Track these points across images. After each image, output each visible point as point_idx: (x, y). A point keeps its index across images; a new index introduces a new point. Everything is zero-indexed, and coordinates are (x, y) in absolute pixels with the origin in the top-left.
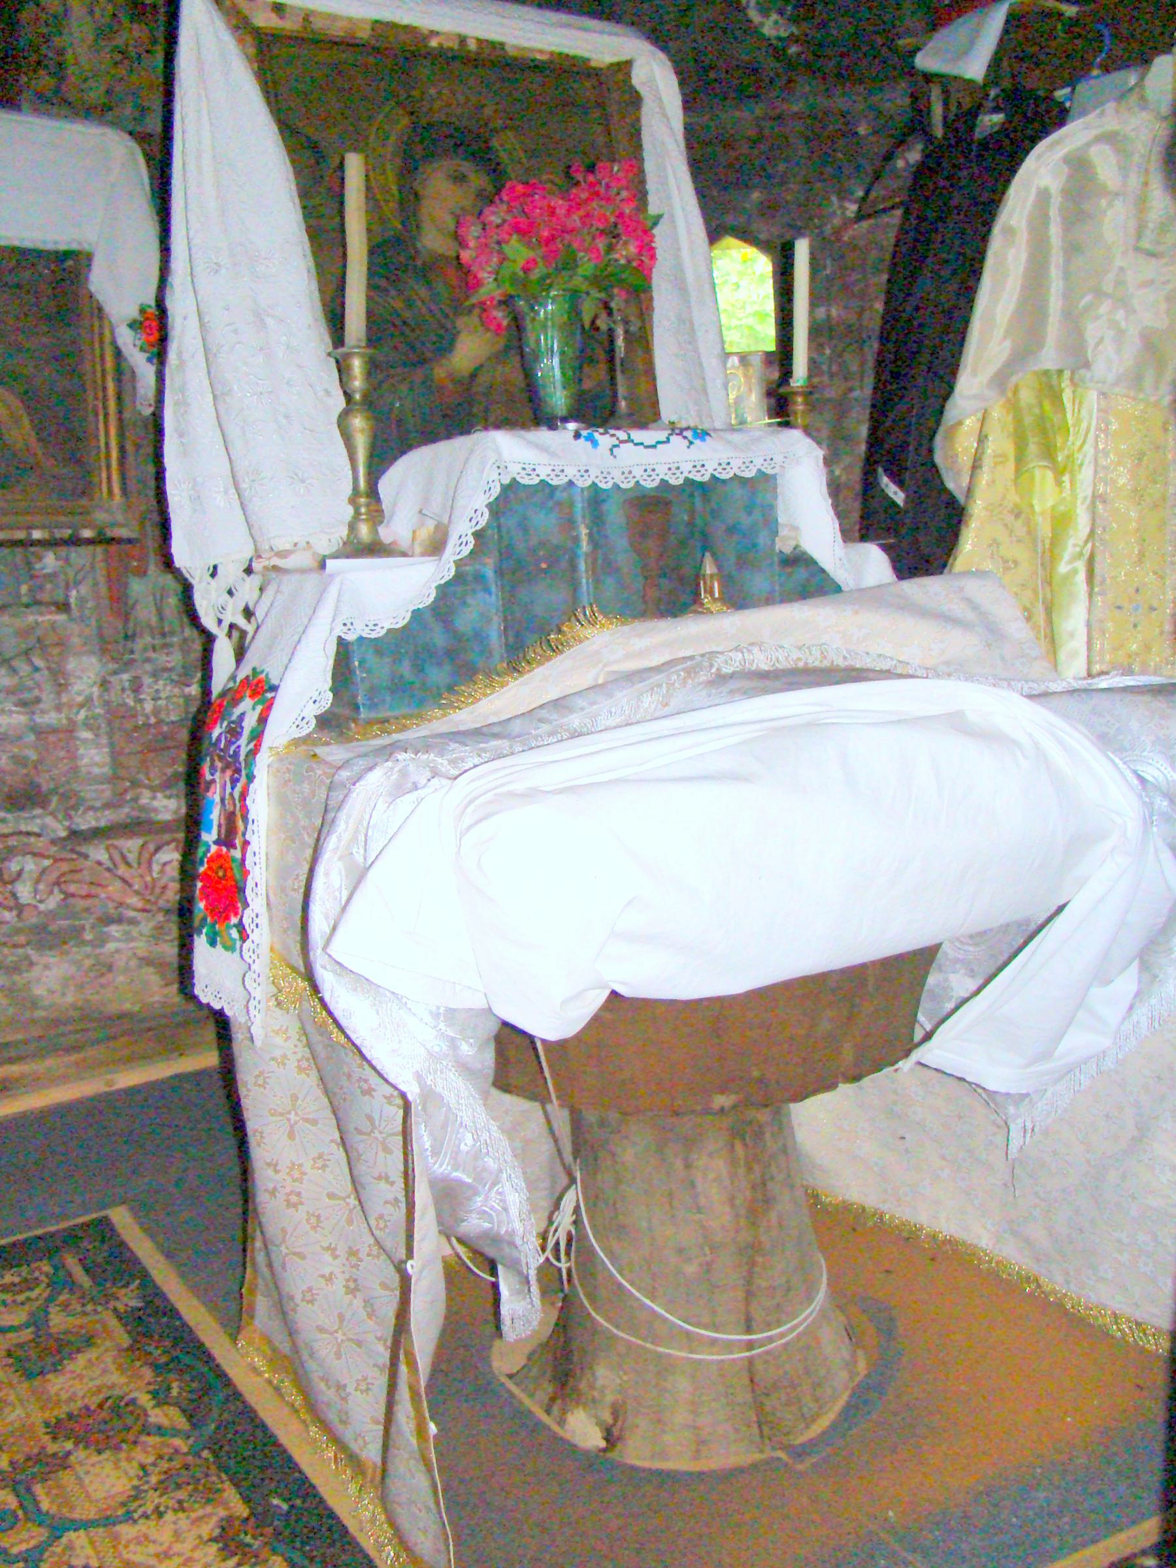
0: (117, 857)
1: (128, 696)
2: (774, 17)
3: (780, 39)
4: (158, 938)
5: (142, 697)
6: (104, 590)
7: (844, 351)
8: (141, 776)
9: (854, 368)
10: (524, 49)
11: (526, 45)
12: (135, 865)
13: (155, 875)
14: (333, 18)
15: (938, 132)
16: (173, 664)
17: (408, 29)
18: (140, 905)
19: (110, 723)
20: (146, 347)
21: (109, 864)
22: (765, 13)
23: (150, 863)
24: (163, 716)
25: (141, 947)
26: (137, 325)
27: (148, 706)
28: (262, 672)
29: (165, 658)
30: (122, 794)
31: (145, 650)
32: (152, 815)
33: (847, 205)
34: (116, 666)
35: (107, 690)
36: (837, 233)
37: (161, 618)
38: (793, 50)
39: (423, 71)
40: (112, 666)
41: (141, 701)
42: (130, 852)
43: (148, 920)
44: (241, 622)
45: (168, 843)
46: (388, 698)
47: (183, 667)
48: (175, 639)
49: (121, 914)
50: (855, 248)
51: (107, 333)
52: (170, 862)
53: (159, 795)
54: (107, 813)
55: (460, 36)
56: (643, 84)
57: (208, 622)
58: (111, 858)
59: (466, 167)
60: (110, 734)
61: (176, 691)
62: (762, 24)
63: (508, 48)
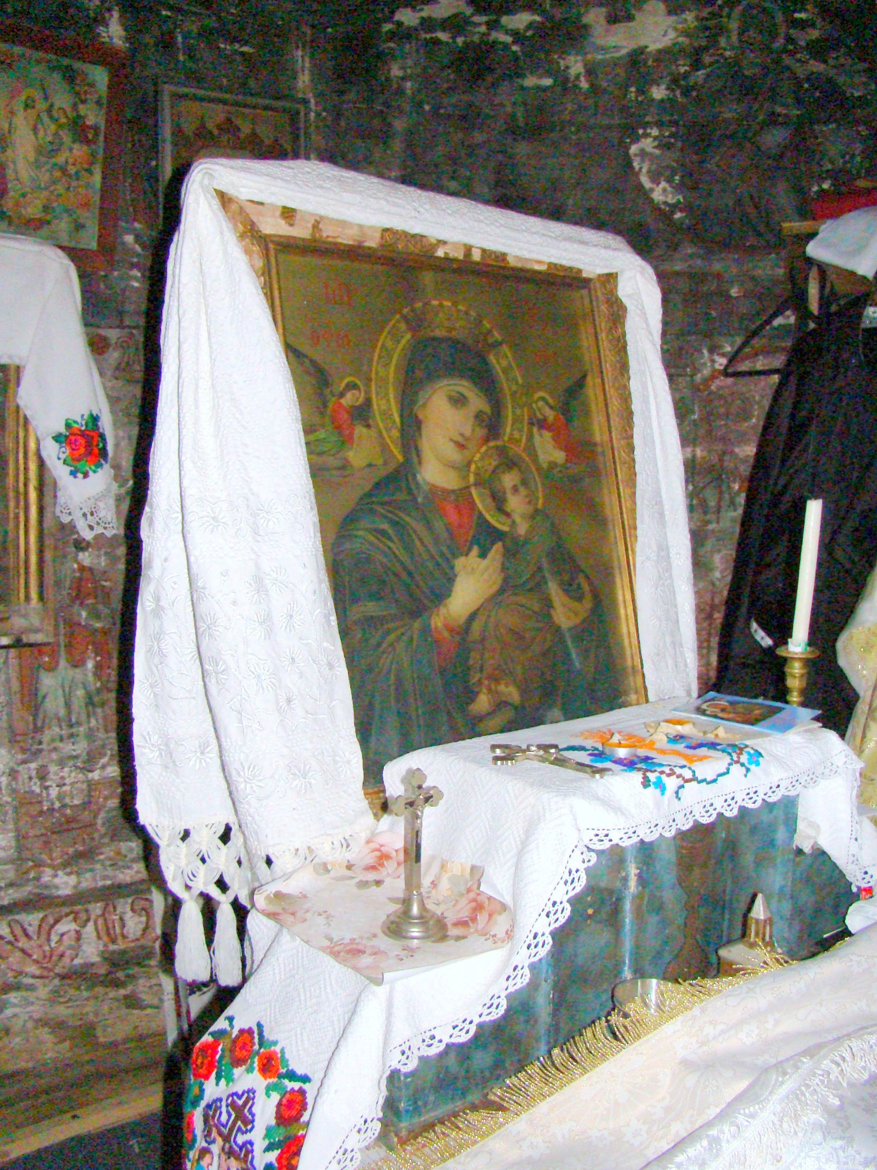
0: (18, 931)
1: (35, 784)
2: (663, 184)
3: (665, 203)
4: (54, 1001)
5: (48, 784)
6: (15, 686)
7: (704, 487)
8: (44, 857)
9: (712, 503)
10: (527, 260)
11: (527, 256)
12: (35, 938)
13: (53, 944)
14: (343, 224)
15: (814, 306)
16: (79, 752)
17: (419, 238)
18: (38, 972)
19: (16, 810)
20: (69, 461)
21: (10, 937)
22: (656, 180)
23: (49, 934)
24: (67, 800)
25: (37, 1010)
26: (63, 439)
27: (54, 792)
28: (275, 1043)
29: (71, 747)
30: (25, 873)
31: (53, 740)
32: (54, 891)
33: (716, 358)
34: (24, 756)
35: (15, 779)
36: (707, 382)
37: (68, 705)
38: (678, 215)
39: (428, 278)
40: (20, 757)
41: (47, 788)
42: (30, 925)
43: (45, 986)
44: (214, 892)
45: (67, 915)
46: (432, 1098)
47: (88, 754)
48: (82, 729)
49: (19, 982)
50: (721, 397)
51: (32, 445)
52: (69, 931)
53: (60, 873)
54: (11, 891)
55: (465, 245)
56: (629, 296)
57: (175, 887)
58: (12, 932)
59: (464, 387)
60: (17, 820)
61: (81, 776)
62: (652, 190)
63: (509, 259)
